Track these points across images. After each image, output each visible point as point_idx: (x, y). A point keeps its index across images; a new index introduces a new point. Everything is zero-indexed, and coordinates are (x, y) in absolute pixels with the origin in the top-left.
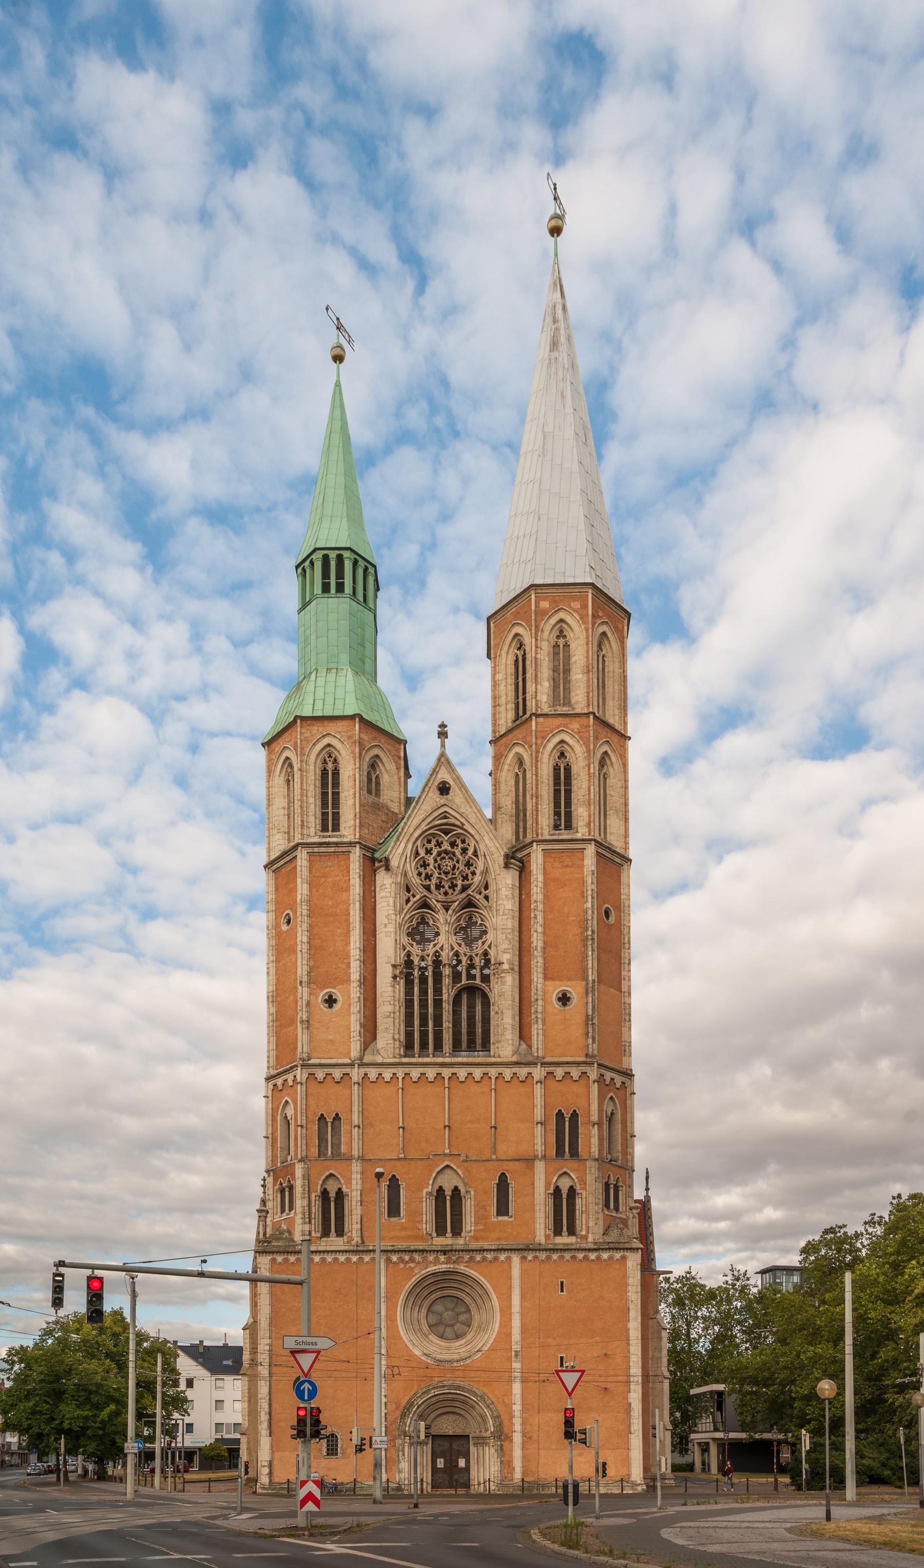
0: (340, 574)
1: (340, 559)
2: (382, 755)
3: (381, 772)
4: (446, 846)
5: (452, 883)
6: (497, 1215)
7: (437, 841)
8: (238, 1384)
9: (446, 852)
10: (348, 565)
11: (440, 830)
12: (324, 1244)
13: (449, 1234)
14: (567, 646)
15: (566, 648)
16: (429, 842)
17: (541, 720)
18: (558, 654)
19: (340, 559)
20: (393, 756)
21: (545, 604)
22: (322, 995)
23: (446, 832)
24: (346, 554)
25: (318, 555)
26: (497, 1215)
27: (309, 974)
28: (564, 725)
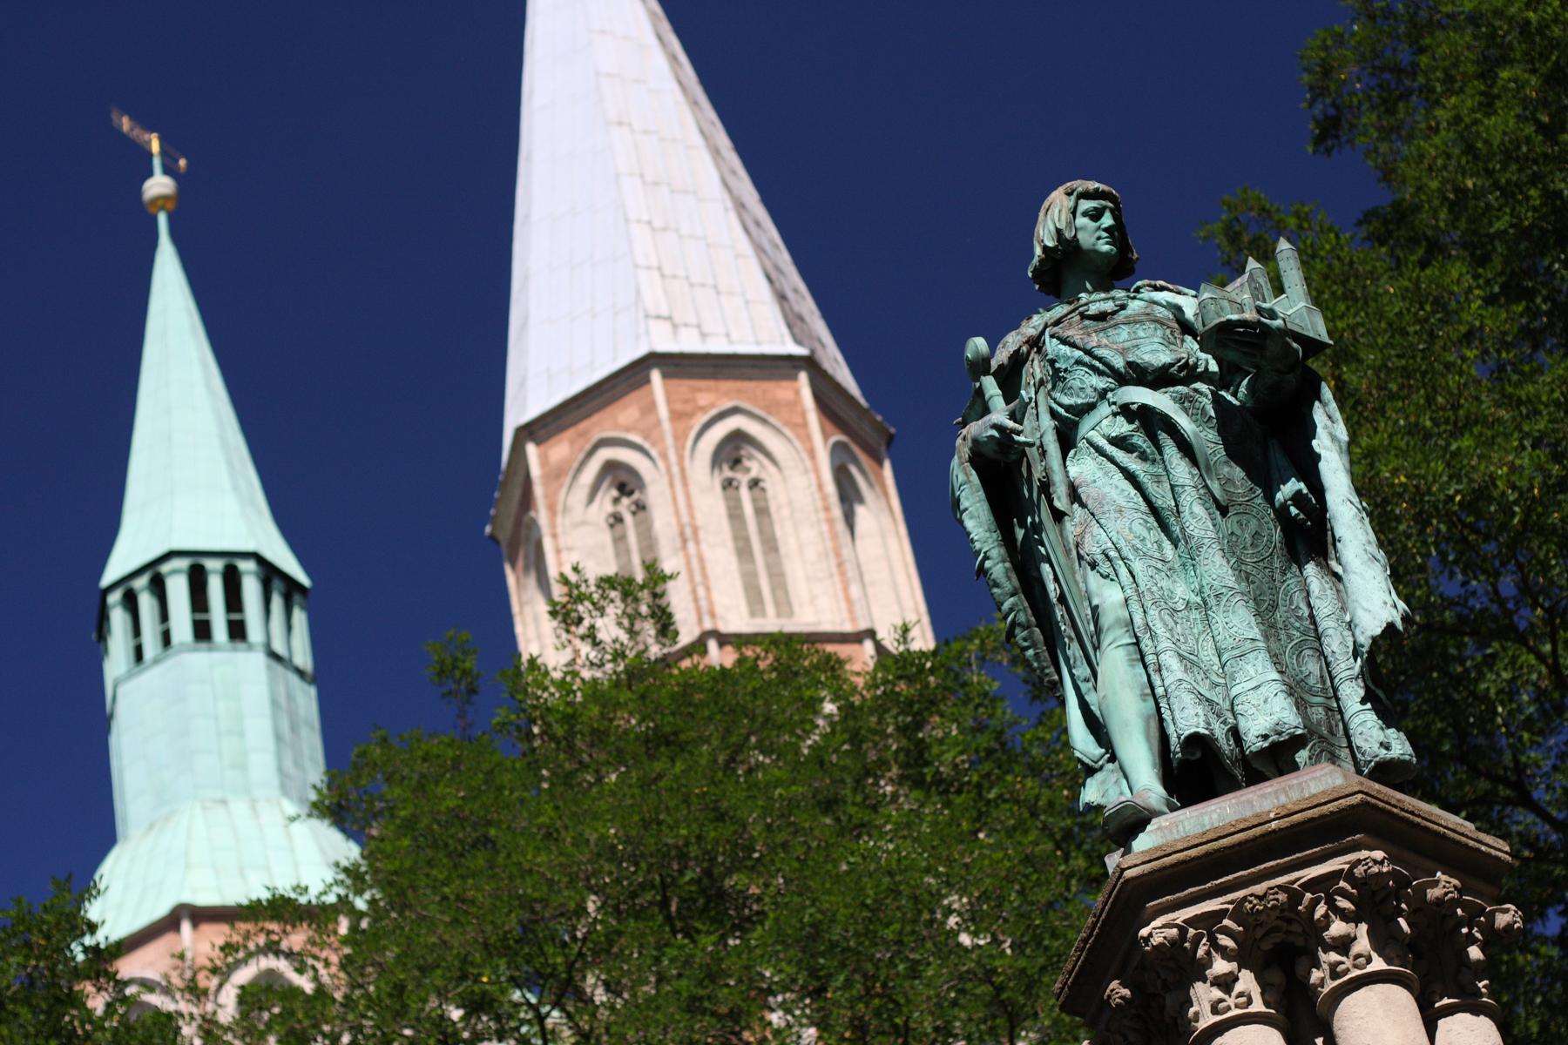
1: (232, 580)
10: (251, 589)
15: (641, 515)
24: (247, 566)
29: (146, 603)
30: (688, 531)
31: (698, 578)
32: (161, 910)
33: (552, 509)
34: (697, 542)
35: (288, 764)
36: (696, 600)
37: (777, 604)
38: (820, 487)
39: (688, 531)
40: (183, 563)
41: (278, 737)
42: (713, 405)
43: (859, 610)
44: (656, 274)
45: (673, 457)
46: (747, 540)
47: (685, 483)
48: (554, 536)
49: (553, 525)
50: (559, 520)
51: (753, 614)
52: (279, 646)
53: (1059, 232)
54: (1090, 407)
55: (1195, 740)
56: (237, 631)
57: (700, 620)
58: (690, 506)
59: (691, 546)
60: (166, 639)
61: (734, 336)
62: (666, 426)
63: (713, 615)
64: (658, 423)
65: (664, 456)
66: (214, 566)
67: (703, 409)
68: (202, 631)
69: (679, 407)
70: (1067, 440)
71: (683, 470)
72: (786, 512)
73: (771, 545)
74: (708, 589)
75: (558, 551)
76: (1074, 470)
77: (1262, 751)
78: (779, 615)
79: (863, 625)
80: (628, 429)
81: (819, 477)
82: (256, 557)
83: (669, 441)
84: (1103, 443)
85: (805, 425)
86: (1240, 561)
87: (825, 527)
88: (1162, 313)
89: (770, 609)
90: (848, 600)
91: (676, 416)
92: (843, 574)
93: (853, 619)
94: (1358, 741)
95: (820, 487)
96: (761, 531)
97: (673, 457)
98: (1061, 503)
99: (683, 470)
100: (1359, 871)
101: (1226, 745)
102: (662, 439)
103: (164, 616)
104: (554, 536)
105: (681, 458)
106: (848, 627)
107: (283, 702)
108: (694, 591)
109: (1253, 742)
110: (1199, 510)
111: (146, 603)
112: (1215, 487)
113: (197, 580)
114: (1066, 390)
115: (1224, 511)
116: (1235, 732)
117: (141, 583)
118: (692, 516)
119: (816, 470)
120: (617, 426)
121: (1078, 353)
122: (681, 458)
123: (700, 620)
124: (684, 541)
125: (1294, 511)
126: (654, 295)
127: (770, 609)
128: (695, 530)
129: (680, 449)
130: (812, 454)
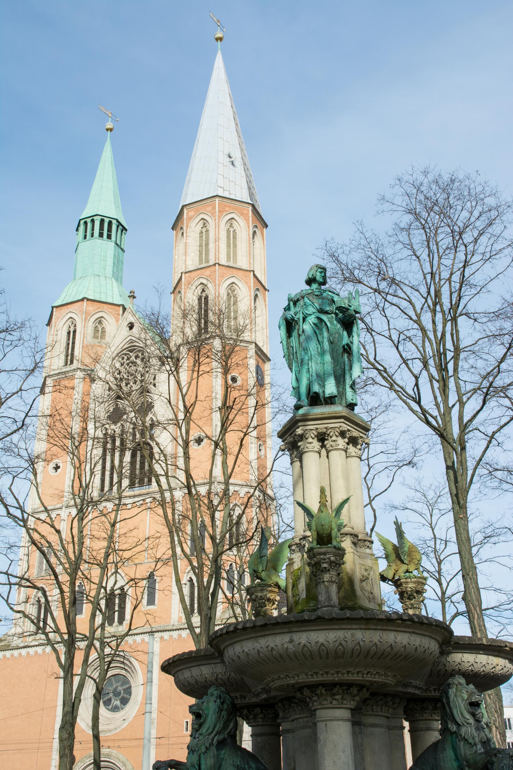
0: (110, 230)
1: (110, 223)
2: (105, 315)
3: (106, 325)
4: (133, 358)
5: (135, 380)
6: (147, 605)
7: (128, 357)
8: (490, 636)
9: (133, 363)
10: (114, 227)
11: (128, 351)
12: (110, 630)
13: (115, 624)
14: (207, 231)
15: (207, 232)
16: (123, 359)
17: (188, 274)
18: (202, 237)
19: (110, 223)
20: (113, 315)
21: (191, 213)
22: (52, 465)
23: (131, 351)
24: (114, 222)
25: (82, 222)
26: (147, 605)
27: (115, 453)
28: (201, 274)
29: (89, 225)
30: (217, 239)
31: (217, 250)
32: (80, 298)
33: (187, 226)
34: (219, 242)
35: (115, 270)
36: (215, 255)
37: (233, 260)
38: (249, 235)
39: (217, 239)
40: (99, 218)
41: (114, 263)
42: (229, 211)
43: (252, 265)
44: (222, 176)
45: (217, 220)
46: (230, 243)
47: (219, 228)
48: (186, 233)
49: (187, 230)
50: (188, 229)
51: (227, 261)
52: (118, 242)
53: (313, 275)
54: (310, 315)
55: (315, 393)
56: (109, 237)
57: (215, 260)
58: (219, 233)
59: (217, 242)
60: (92, 235)
61: (237, 195)
62: (217, 213)
63: (219, 260)
64: (216, 212)
65: (215, 220)
66: (107, 220)
67: (226, 211)
68: (101, 235)
69: (221, 209)
70: (304, 320)
71: (219, 224)
72: (240, 239)
73: (235, 245)
74: (219, 253)
75: (187, 236)
76: (304, 327)
77: (328, 397)
78: (233, 263)
79: (252, 269)
80: (208, 212)
81: (249, 233)
82: (118, 221)
83: (217, 217)
84: (311, 323)
85: (249, 220)
86: (333, 355)
87: (248, 245)
88: (329, 297)
89: (232, 261)
90: (250, 263)
91: (220, 211)
92: (250, 256)
93: (250, 267)
94: (347, 397)
95: (249, 235)
96: (233, 242)
97: (217, 220)
98: (300, 332)
99: (219, 224)
100: (341, 429)
101: (321, 395)
102: (216, 216)
103: (93, 229)
104: (186, 233)
105: (219, 221)
106: (248, 269)
107: (117, 256)
108: (215, 253)
109: (327, 395)
110: (327, 343)
111: (89, 225)
112: (331, 338)
113: (102, 222)
114: (306, 309)
115: (332, 343)
116: (324, 392)
117: (89, 220)
118: (219, 236)
119: (249, 231)
120: (206, 211)
121: (311, 303)
122: (219, 221)
123: (215, 260)
124: (216, 241)
125: (346, 347)
126: (221, 183)
127: (232, 261)
128: (219, 239)
129: (219, 219)
130: (249, 227)
